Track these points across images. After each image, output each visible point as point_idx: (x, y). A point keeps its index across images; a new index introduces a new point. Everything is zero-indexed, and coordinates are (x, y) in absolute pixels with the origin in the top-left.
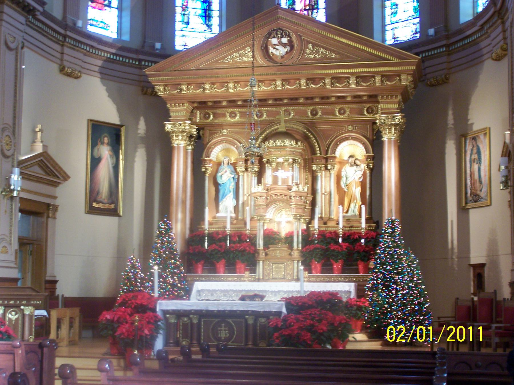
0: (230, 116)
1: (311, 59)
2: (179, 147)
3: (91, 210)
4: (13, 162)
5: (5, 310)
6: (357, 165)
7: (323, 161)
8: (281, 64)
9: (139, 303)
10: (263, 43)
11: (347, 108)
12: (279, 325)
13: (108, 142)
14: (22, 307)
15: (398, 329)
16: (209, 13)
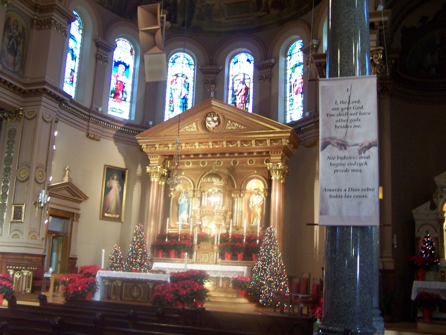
0: (187, 164)
1: (229, 130)
2: (154, 182)
3: (103, 218)
4: (44, 187)
5: (14, 272)
6: (259, 195)
7: (239, 192)
8: (213, 133)
9: (87, 271)
10: (203, 121)
11: (254, 159)
12: (160, 289)
13: (117, 178)
14: (22, 271)
16: (185, 105)
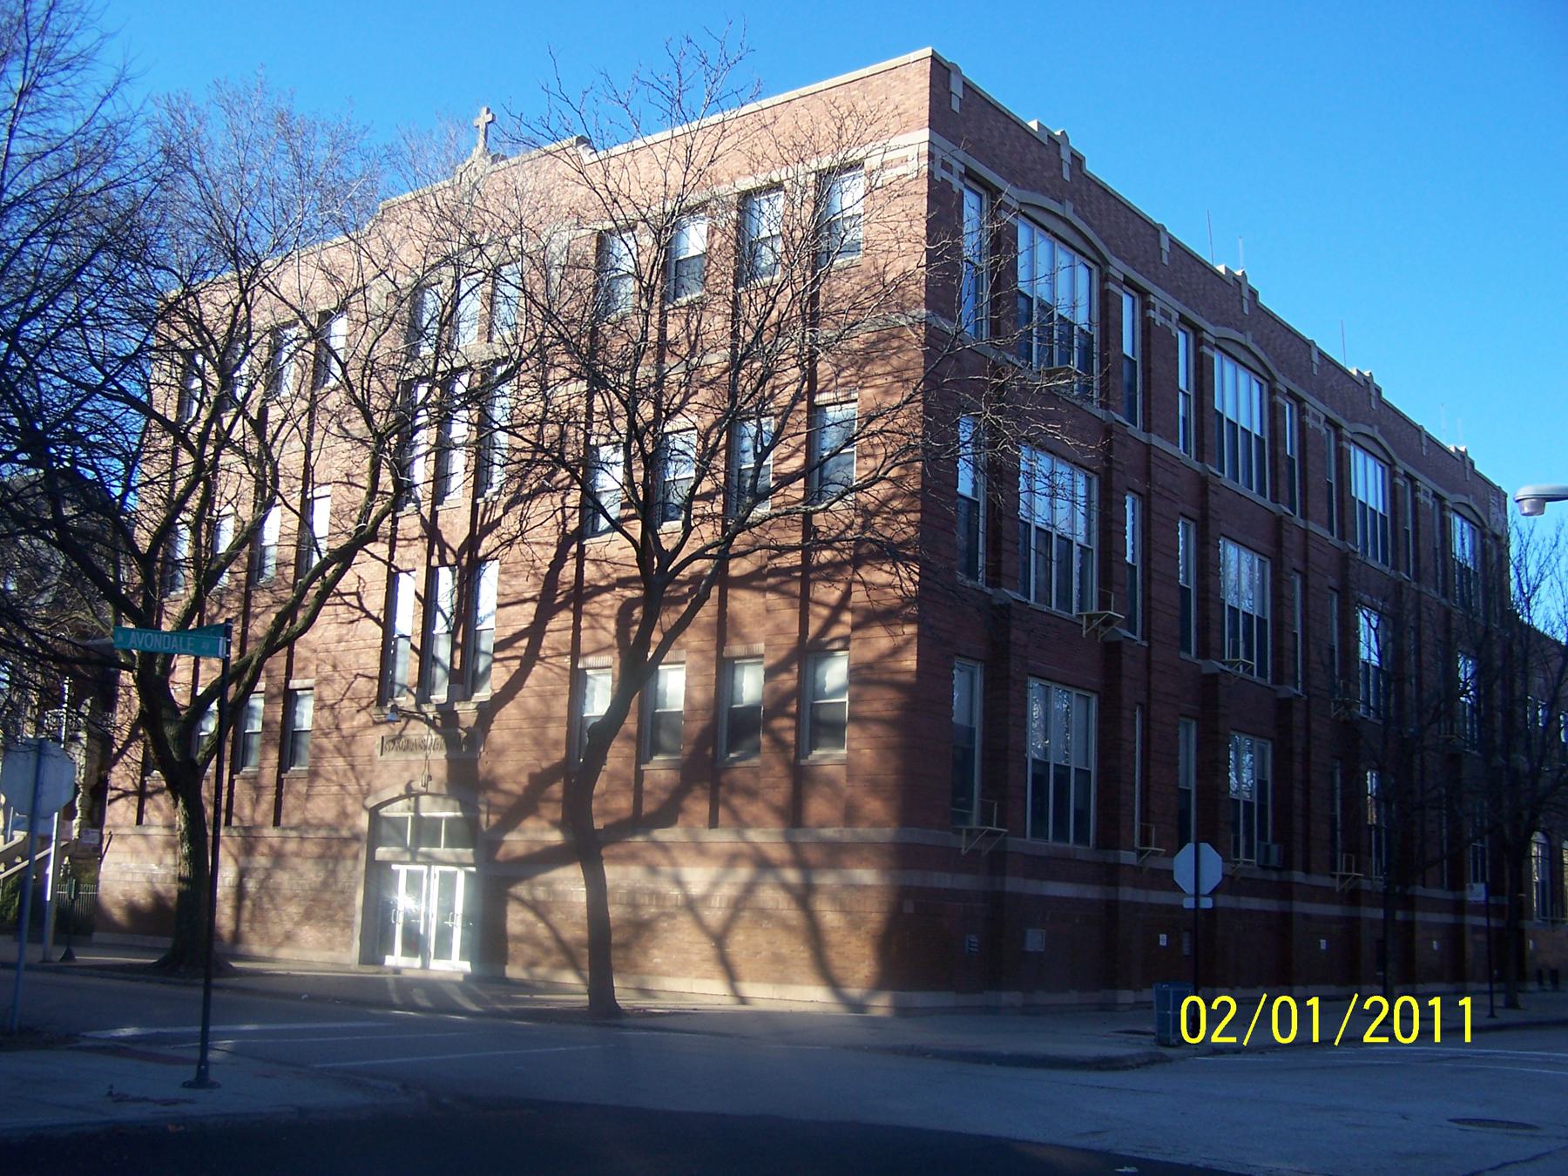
15: (1215, 1006)
